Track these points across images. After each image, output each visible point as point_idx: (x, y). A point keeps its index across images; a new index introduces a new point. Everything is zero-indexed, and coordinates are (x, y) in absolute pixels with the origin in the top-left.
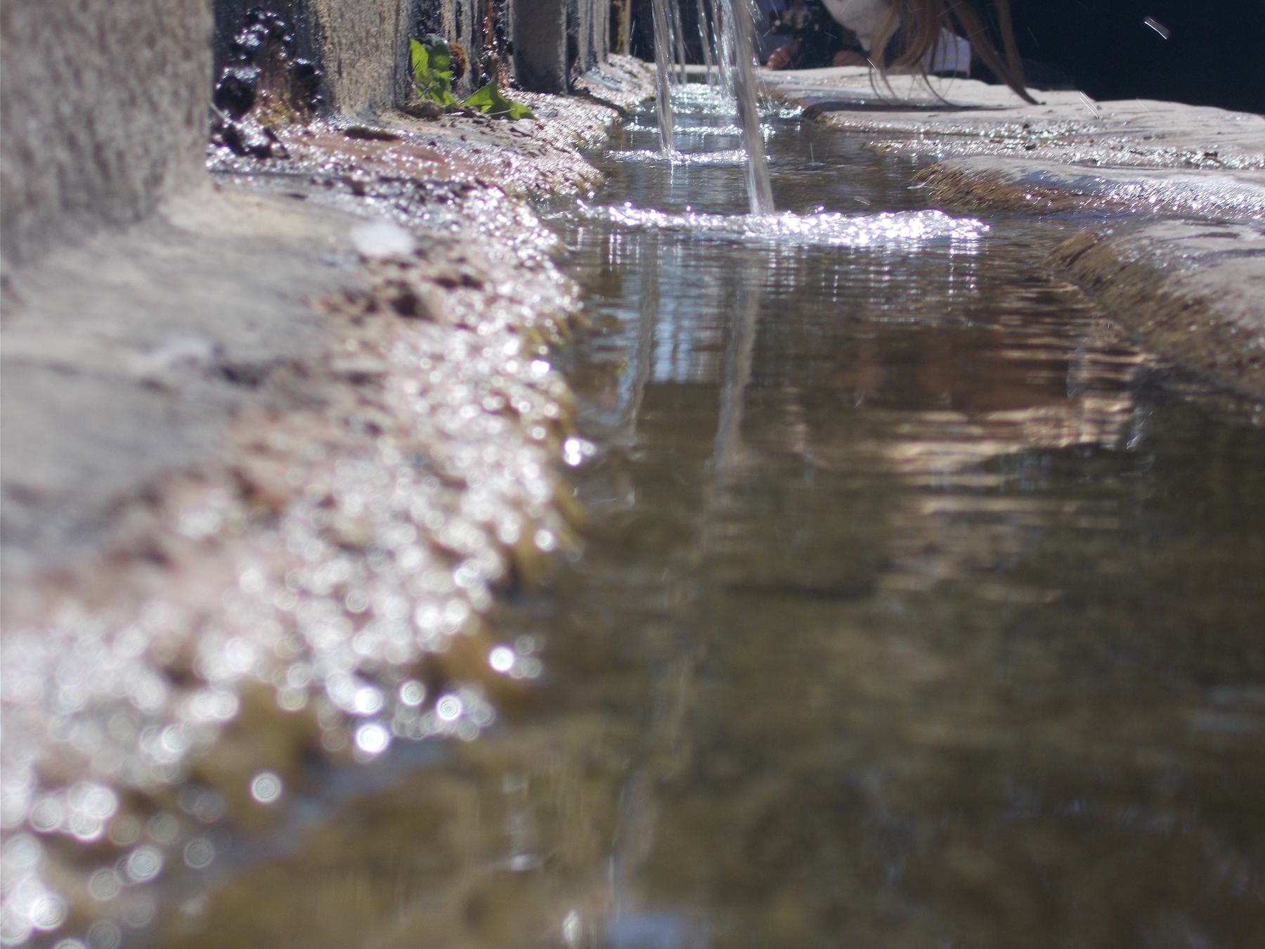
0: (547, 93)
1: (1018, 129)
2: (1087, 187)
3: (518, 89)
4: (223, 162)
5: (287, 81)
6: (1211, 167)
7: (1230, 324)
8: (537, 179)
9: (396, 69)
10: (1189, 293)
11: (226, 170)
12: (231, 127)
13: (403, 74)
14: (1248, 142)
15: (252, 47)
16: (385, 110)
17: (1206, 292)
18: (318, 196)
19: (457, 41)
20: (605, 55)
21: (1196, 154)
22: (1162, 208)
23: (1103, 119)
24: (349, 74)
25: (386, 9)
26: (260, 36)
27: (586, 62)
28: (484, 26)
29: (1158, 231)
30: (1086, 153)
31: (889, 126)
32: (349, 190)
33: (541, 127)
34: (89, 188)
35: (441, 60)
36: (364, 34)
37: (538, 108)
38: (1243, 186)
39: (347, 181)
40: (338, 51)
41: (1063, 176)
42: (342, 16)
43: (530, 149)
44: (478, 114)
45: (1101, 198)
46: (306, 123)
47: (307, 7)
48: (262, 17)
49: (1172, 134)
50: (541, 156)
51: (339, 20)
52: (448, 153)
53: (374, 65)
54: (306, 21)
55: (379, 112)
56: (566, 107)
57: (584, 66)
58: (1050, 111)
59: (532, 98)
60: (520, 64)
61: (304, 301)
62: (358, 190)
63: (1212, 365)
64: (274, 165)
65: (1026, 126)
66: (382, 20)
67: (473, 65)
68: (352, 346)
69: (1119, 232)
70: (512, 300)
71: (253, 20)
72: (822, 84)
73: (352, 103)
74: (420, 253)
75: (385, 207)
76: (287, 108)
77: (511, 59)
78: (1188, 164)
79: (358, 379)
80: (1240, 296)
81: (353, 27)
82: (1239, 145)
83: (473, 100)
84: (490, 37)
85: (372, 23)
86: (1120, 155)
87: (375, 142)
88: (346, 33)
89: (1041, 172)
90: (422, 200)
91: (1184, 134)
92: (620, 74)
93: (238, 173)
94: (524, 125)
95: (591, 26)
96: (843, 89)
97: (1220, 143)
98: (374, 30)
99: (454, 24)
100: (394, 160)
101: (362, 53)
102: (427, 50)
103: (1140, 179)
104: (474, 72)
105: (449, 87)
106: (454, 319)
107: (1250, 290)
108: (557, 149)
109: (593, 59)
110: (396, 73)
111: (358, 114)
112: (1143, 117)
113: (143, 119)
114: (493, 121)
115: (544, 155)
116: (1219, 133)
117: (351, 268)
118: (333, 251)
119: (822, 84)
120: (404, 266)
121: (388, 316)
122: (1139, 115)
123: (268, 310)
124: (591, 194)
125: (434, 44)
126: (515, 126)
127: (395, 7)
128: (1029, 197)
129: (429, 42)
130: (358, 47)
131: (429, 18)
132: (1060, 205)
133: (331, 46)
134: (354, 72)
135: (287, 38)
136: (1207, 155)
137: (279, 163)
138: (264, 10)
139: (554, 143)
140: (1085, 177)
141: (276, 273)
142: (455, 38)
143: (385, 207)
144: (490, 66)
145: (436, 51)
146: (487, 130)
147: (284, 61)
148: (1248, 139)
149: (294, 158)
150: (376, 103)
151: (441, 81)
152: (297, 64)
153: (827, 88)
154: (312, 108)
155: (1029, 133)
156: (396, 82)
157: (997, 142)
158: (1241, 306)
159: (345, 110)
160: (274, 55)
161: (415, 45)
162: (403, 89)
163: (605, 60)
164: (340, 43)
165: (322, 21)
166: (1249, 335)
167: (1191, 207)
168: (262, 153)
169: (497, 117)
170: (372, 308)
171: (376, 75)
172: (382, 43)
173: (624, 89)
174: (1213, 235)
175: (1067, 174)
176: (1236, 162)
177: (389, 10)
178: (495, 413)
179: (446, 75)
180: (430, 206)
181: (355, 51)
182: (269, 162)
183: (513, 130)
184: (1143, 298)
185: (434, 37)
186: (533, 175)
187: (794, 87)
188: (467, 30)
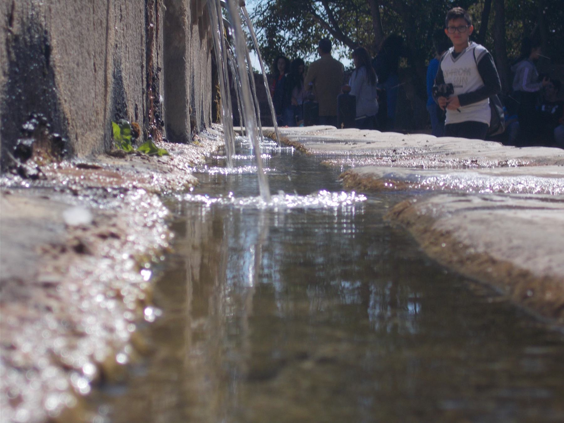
0: (179, 143)
1: (391, 153)
2: (412, 180)
3: (167, 141)
4: (16, 183)
5: (49, 144)
6: (475, 167)
7: (460, 243)
8: (165, 184)
9: (105, 136)
10: (444, 228)
11: (17, 186)
12: (21, 167)
14: (490, 155)
15: (31, 130)
16: (100, 154)
17: (451, 228)
18: (57, 197)
19: (136, 122)
20: (210, 124)
21: (467, 161)
22: (446, 187)
23: (429, 146)
24: (81, 139)
25: (99, 109)
26: (35, 125)
27: (200, 128)
28: (149, 114)
29: (436, 200)
30: (419, 163)
31: (333, 153)
32: (71, 193)
33: (172, 159)
35: (126, 131)
36: (88, 121)
37: (174, 150)
38: (481, 176)
39: (71, 189)
40: (75, 129)
41: (401, 175)
42: (77, 113)
43: (164, 170)
44: (143, 154)
45: (418, 184)
46: (59, 162)
47: (59, 110)
48: (35, 116)
49: (458, 152)
50: (169, 172)
51: (76, 115)
52: (123, 174)
53: (94, 134)
54: (59, 117)
55: (96, 155)
56: (187, 149)
57: (199, 130)
58: (406, 144)
59: (173, 146)
60: (169, 130)
61: (33, 248)
62: (75, 193)
63: (451, 262)
64: (40, 183)
65: (395, 151)
66: (97, 114)
67: (144, 132)
68: (50, 269)
69: (419, 201)
70: (134, 243)
71: (31, 117)
72: (307, 134)
73: (84, 152)
74: (94, 223)
75: (273, 153)
76: (49, 156)
77: (164, 128)
78: (464, 167)
79: (48, 285)
80: (465, 229)
81: (83, 118)
82: (487, 156)
83: (142, 148)
84: (152, 119)
85: (92, 116)
86: (433, 163)
87: (90, 170)
88: (79, 121)
89: (392, 173)
90: (105, 197)
91: (464, 152)
92: (217, 132)
93: (23, 188)
94: (165, 158)
95: (202, 112)
96: (317, 136)
97: (478, 156)
98: (93, 119)
99: (134, 114)
100: (96, 178)
101: (87, 129)
102: (120, 127)
103: (436, 175)
104: (145, 135)
105: (130, 143)
106: (103, 253)
107: (470, 227)
108: (180, 169)
109: (203, 127)
110: (105, 137)
111: (86, 157)
112: (447, 145)
114: (150, 157)
115: (170, 172)
116: (479, 151)
117: (60, 231)
118: (54, 223)
119: (307, 134)
120: (84, 229)
121: (71, 254)
122: (445, 144)
123: (15, 254)
124: (192, 189)
125: (123, 123)
126: (160, 160)
127: (104, 108)
128: (386, 184)
129: (121, 123)
130: (85, 127)
131: (121, 112)
132: (400, 187)
133: (72, 127)
134: (84, 138)
135: (48, 125)
136: (472, 161)
137: (42, 182)
138: (36, 113)
139: (178, 166)
140: (411, 175)
141: (23, 235)
142: (135, 120)
143: (273, 153)
144: (153, 132)
145: (124, 127)
146: (147, 162)
147: (48, 135)
148: (490, 154)
149: (49, 179)
150: (95, 151)
151: (127, 140)
152: (54, 137)
153: (309, 136)
154: (62, 156)
155: (396, 154)
156: (105, 141)
157: (380, 159)
158: (465, 234)
159: (79, 155)
160: (42, 133)
161: (114, 124)
162: (109, 145)
163: (210, 126)
164: (76, 126)
165: (66, 116)
166: (466, 247)
167: (459, 187)
168: (35, 177)
169: (152, 156)
170: (63, 250)
171: (95, 139)
172: (98, 124)
173: (218, 140)
174: (460, 201)
175: (403, 173)
176: (485, 164)
177: (101, 110)
178: (113, 298)
179: (128, 137)
180: (109, 199)
181: (84, 129)
182: (37, 181)
183: (159, 161)
184: (425, 231)
185: (123, 121)
186: (164, 182)
187: (294, 136)
188: (140, 116)
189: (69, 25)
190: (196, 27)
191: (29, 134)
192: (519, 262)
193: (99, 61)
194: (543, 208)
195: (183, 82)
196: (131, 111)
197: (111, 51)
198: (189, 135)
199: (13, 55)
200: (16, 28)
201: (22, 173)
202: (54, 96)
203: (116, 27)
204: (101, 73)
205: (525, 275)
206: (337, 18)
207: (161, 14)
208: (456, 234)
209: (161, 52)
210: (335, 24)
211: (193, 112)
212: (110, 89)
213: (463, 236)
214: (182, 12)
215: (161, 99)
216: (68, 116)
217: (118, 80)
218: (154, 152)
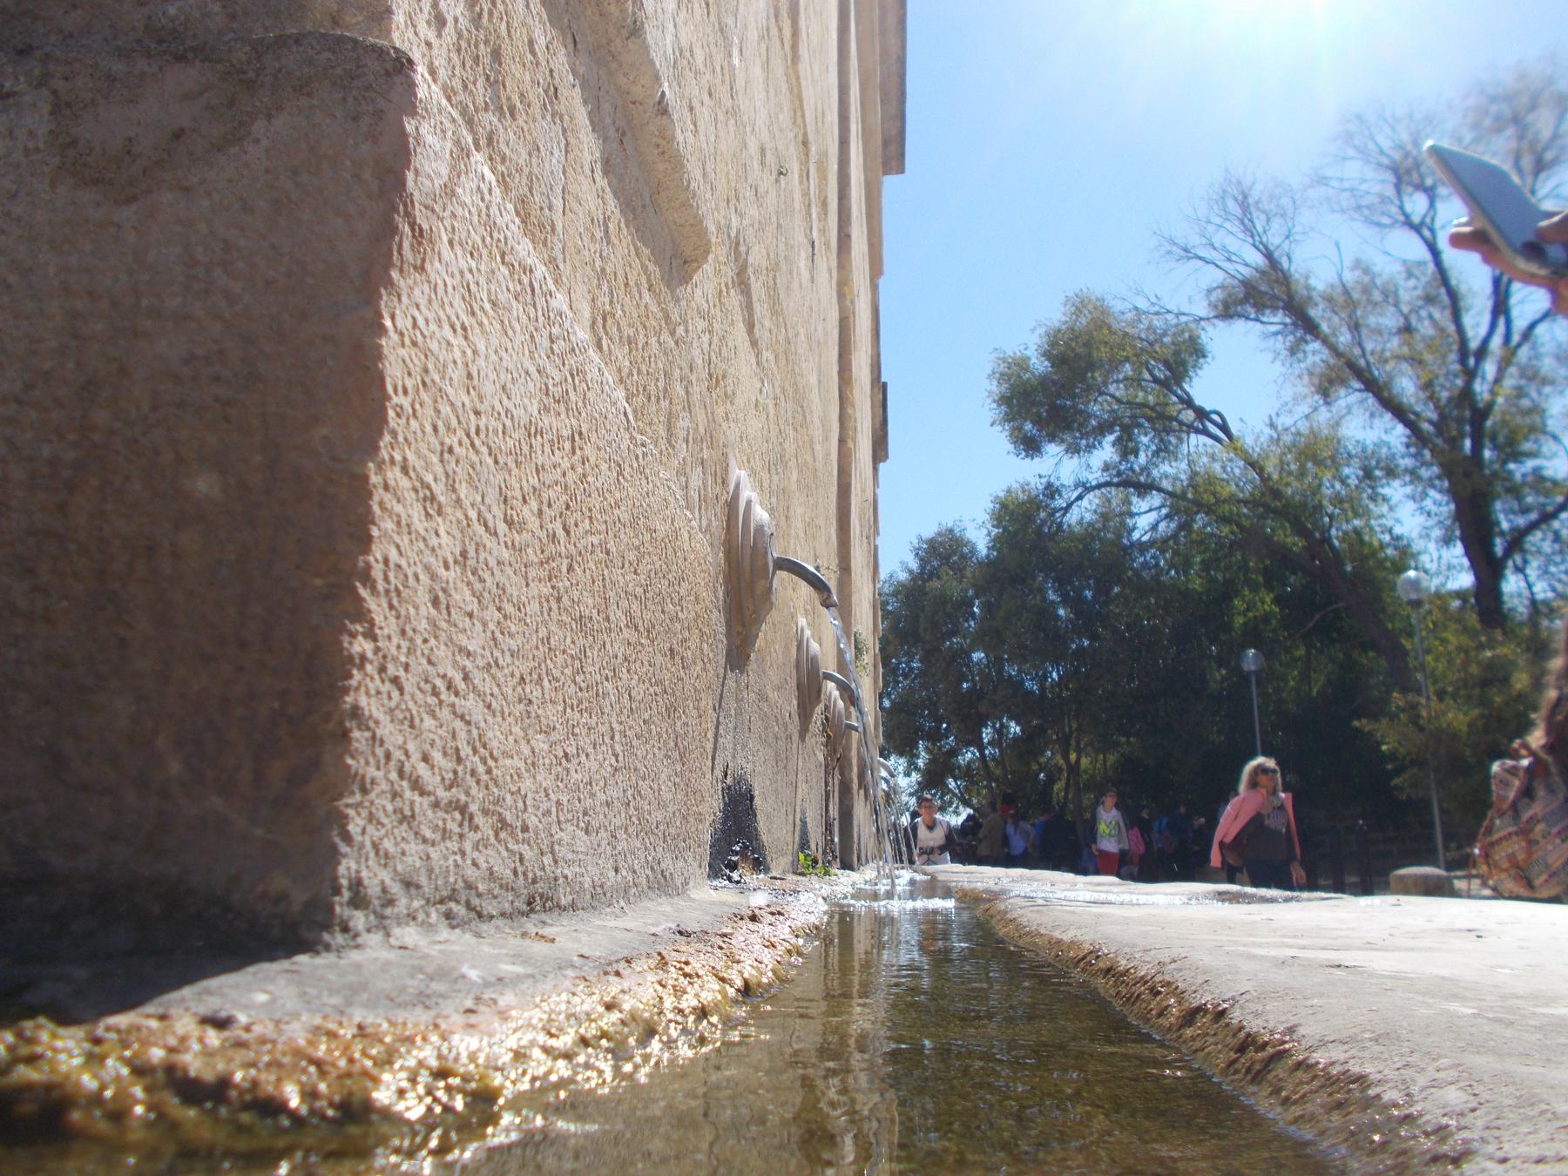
13: (795, 862)
34: (658, 883)
60: (842, 861)
94: (834, 878)
109: (867, 861)
113: (681, 864)
141: (717, 911)
144: (829, 862)
145: (806, 856)
168: (738, 882)
188: (820, 850)
189: (768, 782)
190: (862, 792)
192: (1057, 934)
193: (790, 809)
195: (852, 828)
196: (813, 846)
197: (799, 802)
200: (729, 780)
201: (730, 879)
202: (756, 830)
203: (803, 789)
204: (791, 818)
205: (1059, 942)
207: (836, 782)
209: (837, 807)
211: (859, 850)
212: (798, 829)
213: (1024, 921)
215: (836, 839)
217: (804, 824)
218: (827, 873)
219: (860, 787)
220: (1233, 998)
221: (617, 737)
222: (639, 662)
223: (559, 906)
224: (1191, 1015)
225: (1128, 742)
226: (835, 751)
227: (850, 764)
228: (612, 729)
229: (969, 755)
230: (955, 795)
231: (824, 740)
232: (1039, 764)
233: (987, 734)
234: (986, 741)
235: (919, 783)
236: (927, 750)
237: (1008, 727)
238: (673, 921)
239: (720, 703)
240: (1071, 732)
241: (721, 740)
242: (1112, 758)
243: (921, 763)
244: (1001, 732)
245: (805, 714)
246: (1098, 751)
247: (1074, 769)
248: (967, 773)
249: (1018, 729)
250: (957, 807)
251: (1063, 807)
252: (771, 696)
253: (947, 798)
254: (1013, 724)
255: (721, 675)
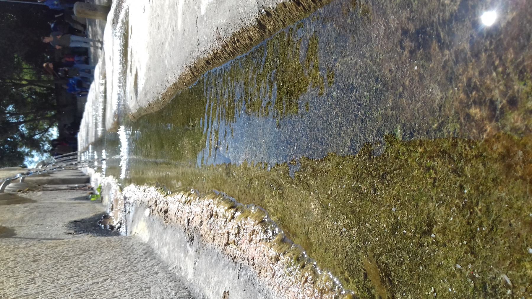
17: (147, 103)
71: (99, 226)
166: (158, 99)
188: (85, 192)
190: (51, 175)
191: (105, 226)
193: (72, 205)
194: (131, 69)
197: (67, 202)
198: (87, 177)
199: (81, 232)
203: (59, 200)
204: (76, 205)
206: (40, 132)
207: (49, 186)
208: (151, 102)
209: (61, 186)
210: (43, 132)
214: (47, 180)
215: (77, 185)
216: (94, 214)
217: (76, 199)
219: (49, 176)
220: (259, 8)
221: (96, 281)
222: (51, 276)
223: (190, 294)
224: (261, 26)
225: (17, 58)
226: (35, 187)
227: (40, 180)
228: (93, 284)
229: (23, 129)
230: (43, 135)
231: (31, 192)
232: (28, 97)
233: (13, 120)
234: (16, 121)
235: (37, 151)
236: (21, 147)
237: (10, 110)
238: (186, 244)
239: (35, 239)
240: (12, 82)
241: (54, 237)
242: (25, 66)
243: (27, 150)
244: (11, 114)
245: (22, 201)
246: (21, 71)
247: (30, 82)
248: (33, 130)
249: (10, 106)
250: (49, 135)
251: (48, 89)
252: (19, 216)
253: (44, 139)
254: (8, 109)
255: (20, 239)
